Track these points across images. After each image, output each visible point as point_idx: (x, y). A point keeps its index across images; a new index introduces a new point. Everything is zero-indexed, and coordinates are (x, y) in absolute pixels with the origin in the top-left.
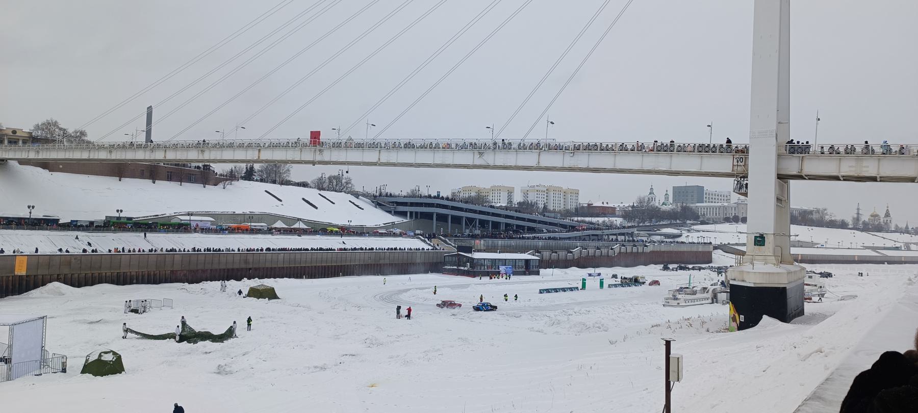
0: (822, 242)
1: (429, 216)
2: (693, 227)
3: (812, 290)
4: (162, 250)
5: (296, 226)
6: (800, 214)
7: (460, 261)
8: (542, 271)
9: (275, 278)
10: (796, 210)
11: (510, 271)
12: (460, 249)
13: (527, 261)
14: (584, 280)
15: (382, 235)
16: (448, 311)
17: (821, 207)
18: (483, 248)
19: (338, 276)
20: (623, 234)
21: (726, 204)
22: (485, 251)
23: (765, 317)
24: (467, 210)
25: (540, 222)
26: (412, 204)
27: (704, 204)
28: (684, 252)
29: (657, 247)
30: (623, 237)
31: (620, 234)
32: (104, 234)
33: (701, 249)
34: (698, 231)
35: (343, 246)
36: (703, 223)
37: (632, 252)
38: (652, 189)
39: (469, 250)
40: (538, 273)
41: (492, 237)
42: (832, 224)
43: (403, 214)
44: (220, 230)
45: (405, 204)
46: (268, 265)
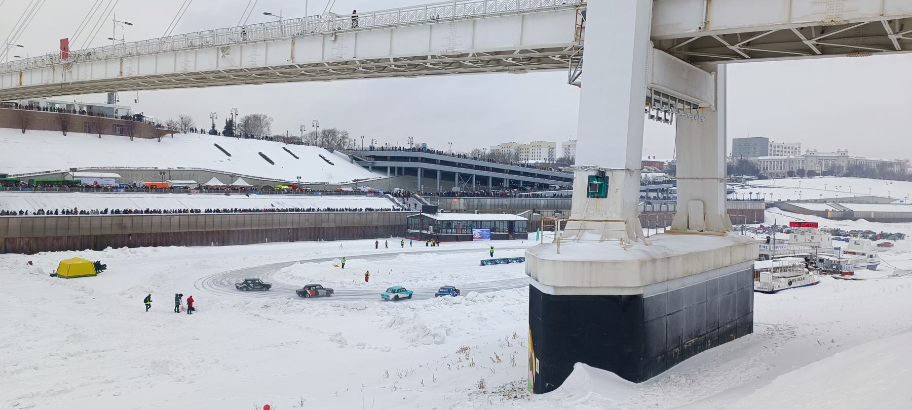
0: (902, 198)
1: (412, 172)
2: (750, 183)
3: (857, 261)
4: (56, 212)
5: (236, 184)
6: (878, 166)
7: (423, 223)
8: (530, 235)
9: (155, 246)
10: (874, 162)
11: (488, 234)
12: (426, 209)
13: (511, 224)
15: (347, 193)
16: (255, 298)
17: (902, 158)
18: (462, 207)
19: (263, 241)
21: (792, 157)
22: (465, 211)
23: (579, 367)
25: (553, 178)
26: (393, 159)
30: (655, 194)
32: (45, 194)
33: (749, 206)
36: (761, 177)
37: (660, 212)
39: (433, 210)
40: (526, 237)
43: (383, 170)
44: (131, 188)
45: (384, 158)
46: (156, 230)
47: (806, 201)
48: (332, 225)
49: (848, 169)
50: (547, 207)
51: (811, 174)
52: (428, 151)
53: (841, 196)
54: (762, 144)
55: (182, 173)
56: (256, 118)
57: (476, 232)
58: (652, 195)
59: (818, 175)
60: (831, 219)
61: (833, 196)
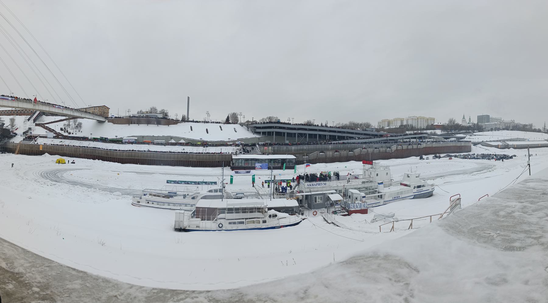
1: (269, 133)
8: (297, 166)
14: (231, 176)
18: (270, 151)
20: (415, 138)
22: (274, 154)
24: (276, 127)
25: (356, 134)
28: (450, 147)
29: (429, 145)
30: (414, 140)
31: (412, 138)
35: (183, 151)
41: (308, 144)
42: (535, 131)
45: (259, 128)
47: (491, 141)
48: (195, 160)
50: (332, 149)
51: (498, 129)
52: (282, 123)
54: (487, 118)
55: (158, 138)
56: (233, 114)
57: (258, 165)
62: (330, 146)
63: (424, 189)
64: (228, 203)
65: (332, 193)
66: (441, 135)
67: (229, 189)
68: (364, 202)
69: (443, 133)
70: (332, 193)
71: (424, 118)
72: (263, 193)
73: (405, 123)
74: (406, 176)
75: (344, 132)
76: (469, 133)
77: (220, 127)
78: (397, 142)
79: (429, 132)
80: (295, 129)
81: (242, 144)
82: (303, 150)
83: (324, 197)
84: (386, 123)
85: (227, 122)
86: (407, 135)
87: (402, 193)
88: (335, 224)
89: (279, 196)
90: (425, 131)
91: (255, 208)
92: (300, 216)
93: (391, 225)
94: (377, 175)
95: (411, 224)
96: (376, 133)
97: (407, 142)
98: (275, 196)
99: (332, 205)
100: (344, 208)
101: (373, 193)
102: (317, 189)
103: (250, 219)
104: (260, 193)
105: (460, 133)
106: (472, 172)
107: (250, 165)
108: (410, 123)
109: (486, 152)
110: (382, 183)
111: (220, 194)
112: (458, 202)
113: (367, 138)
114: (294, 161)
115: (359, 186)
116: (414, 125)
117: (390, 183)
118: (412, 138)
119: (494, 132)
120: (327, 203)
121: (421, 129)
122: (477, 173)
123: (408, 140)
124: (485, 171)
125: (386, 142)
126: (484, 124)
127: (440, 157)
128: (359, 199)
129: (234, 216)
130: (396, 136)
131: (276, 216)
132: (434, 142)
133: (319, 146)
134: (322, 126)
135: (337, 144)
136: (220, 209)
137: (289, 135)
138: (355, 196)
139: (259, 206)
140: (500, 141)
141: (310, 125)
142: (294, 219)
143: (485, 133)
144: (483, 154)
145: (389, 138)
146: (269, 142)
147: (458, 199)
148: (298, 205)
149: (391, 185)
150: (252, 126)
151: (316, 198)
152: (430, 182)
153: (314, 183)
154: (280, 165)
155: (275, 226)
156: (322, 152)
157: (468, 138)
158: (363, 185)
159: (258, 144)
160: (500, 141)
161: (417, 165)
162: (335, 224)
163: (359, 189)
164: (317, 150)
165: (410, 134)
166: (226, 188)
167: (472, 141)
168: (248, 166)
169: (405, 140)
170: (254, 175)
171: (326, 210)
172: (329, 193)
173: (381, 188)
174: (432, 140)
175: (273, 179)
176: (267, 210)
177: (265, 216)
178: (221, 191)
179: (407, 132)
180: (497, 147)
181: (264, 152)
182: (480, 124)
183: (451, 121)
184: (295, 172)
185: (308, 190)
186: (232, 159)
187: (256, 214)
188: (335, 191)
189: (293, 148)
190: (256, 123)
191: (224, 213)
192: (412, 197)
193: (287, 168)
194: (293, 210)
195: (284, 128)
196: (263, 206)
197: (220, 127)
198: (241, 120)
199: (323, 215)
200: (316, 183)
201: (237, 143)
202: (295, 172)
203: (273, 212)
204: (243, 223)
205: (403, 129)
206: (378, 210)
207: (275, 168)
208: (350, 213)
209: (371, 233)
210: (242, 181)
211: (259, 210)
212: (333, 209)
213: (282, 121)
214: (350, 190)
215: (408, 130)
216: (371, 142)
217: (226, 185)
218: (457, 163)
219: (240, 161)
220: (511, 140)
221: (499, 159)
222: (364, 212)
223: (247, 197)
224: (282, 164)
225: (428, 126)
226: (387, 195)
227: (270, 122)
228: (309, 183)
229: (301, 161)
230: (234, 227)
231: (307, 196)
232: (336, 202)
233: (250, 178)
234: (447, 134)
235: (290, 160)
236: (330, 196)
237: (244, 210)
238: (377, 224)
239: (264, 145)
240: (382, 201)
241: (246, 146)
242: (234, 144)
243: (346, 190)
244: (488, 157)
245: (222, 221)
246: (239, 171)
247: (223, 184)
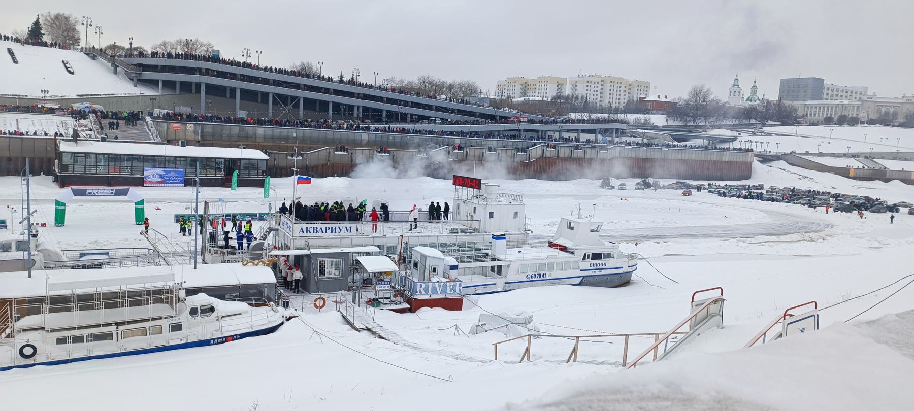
1: (186, 87)
8: (272, 181)
14: (58, 203)
18: (191, 136)
21: (846, 102)
24: (208, 72)
25: (438, 109)
27: (824, 102)
30: (592, 137)
34: (770, 135)
38: (736, 79)
41: (302, 125)
43: (153, 83)
45: (154, 68)
47: (821, 154)
49: (906, 117)
52: (224, 62)
53: (877, 150)
54: (816, 87)
57: (150, 173)
58: (584, 137)
59: (862, 123)
60: (855, 178)
61: (866, 150)
62: (365, 136)
63: (610, 263)
64: (50, 281)
65: (368, 254)
66: (664, 129)
67: (51, 239)
68: (455, 280)
69: (671, 123)
70: (368, 254)
71: (620, 81)
72: (170, 249)
73: (567, 91)
74: (566, 225)
75: (406, 103)
76: (750, 126)
77: (10, 52)
78: (543, 138)
79: (631, 117)
80: (265, 81)
81: (95, 112)
82: (287, 139)
83: (346, 261)
84: (518, 88)
85: (35, 37)
86: (573, 122)
87: (551, 267)
88: (373, 333)
89: (220, 257)
90: (621, 116)
91: (148, 293)
92: (281, 309)
93: (522, 345)
94: (491, 215)
95: (575, 350)
96: (491, 111)
97: (567, 140)
98: (208, 256)
99: (367, 283)
100: (400, 293)
101: (479, 259)
102: (326, 242)
103: (130, 322)
104: (162, 249)
105: (719, 127)
106: (752, 235)
107: (126, 174)
108: (581, 91)
109: (802, 185)
110: (502, 237)
111: (21, 255)
112: (714, 308)
113: (466, 122)
114: (263, 167)
115: (442, 240)
116: (591, 98)
117: (521, 237)
118: (584, 131)
119: (836, 128)
120: (354, 278)
121: (610, 110)
122: (766, 238)
123: (573, 136)
124: (794, 237)
125: (515, 135)
126: (799, 105)
127: (656, 187)
128: (440, 271)
129: (76, 317)
130: (541, 122)
131: (212, 309)
132: (642, 145)
133: (330, 133)
134: (341, 81)
135: (385, 130)
136: (20, 302)
137: (248, 95)
138: (430, 263)
139: (159, 285)
140: (854, 156)
141: (308, 76)
142: (263, 316)
143: (802, 130)
144: (793, 190)
145: (523, 126)
146: (186, 110)
147: (716, 301)
148: (275, 281)
149: (524, 243)
150: (135, 65)
151: (323, 265)
152: (626, 248)
153: (319, 225)
154: (221, 175)
155: (209, 337)
156: (343, 149)
157: (744, 140)
158: (454, 239)
159: (151, 114)
160: (854, 156)
161: (595, 202)
162: (373, 333)
163: (442, 247)
164: (326, 142)
165: (579, 121)
166: (40, 238)
167: (758, 148)
168: (121, 176)
169: (566, 135)
170: (142, 202)
171: (349, 296)
172: (360, 254)
173: (499, 248)
174: (639, 140)
175: (201, 211)
176: (182, 294)
177: (179, 313)
178: (22, 246)
179: (573, 116)
180: (844, 172)
181: (172, 137)
182: (787, 103)
183: (696, 93)
184: (266, 195)
185: (302, 243)
186: (59, 155)
187: (152, 310)
188: (377, 249)
189: (261, 131)
190: (141, 54)
191: (38, 311)
192: (578, 281)
193: (242, 183)
194: (260, 293)
195: (233, 76)
196: (170, 284)
197: (10, 52)
198: (89, 38)
199: (342, 308)
200: (324, 226)
201: (76, 106)
202: (266, 195)
203: (202, 299)
204: (108, 336)
205: (561, 106)
206: (490, 304)
207: (206, 183)
208: (414, 306)
209: (470, 359)
210: (100, 218)
211: (160, 296)
212: (370, 294)
213: (225, 55)
214: (418, 248)
215: (575, 110)
216: (477, 134)
217: (41, 230)
218: (708, 207)
219: (92, 160)
220: (896, 157)
221: (848, 209)
222: (454, 304)
223: (120, 261)
224: (229, 174)
225: (629, 103)
226: (514, 267)
227: (188, 56)
228: (304, 226)
229: (281, 169)
230: (78, 350)
231: (298, 258)
232: (380, 277)
233: (131, 209)
234: (686, 128)
235: (251, 164)
236: (363, 260)
237: (112, 300)
238: (487, 339)
239: (169, 118)
240: (500, 282)
241: (114, 118)
242: (64, 107)
243: (406, 249)
244: (810, 198)
245: (34, 338)
246: (89, 189)
247: (30, 226)
